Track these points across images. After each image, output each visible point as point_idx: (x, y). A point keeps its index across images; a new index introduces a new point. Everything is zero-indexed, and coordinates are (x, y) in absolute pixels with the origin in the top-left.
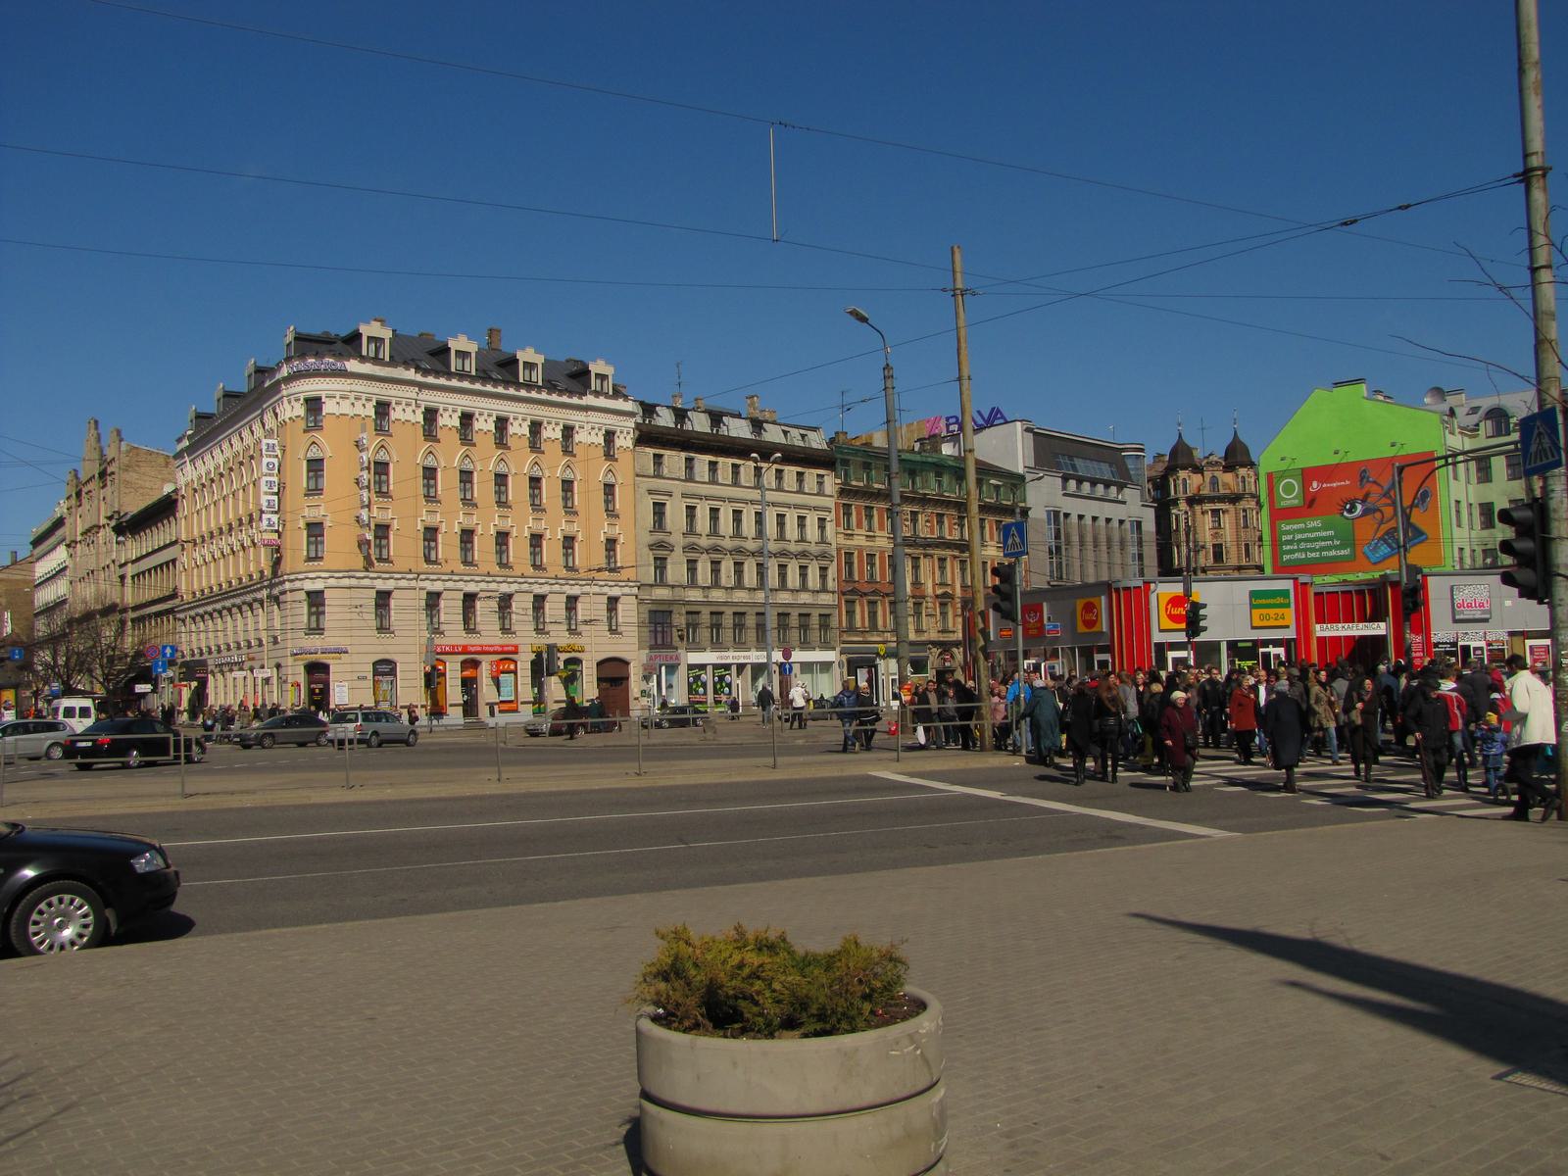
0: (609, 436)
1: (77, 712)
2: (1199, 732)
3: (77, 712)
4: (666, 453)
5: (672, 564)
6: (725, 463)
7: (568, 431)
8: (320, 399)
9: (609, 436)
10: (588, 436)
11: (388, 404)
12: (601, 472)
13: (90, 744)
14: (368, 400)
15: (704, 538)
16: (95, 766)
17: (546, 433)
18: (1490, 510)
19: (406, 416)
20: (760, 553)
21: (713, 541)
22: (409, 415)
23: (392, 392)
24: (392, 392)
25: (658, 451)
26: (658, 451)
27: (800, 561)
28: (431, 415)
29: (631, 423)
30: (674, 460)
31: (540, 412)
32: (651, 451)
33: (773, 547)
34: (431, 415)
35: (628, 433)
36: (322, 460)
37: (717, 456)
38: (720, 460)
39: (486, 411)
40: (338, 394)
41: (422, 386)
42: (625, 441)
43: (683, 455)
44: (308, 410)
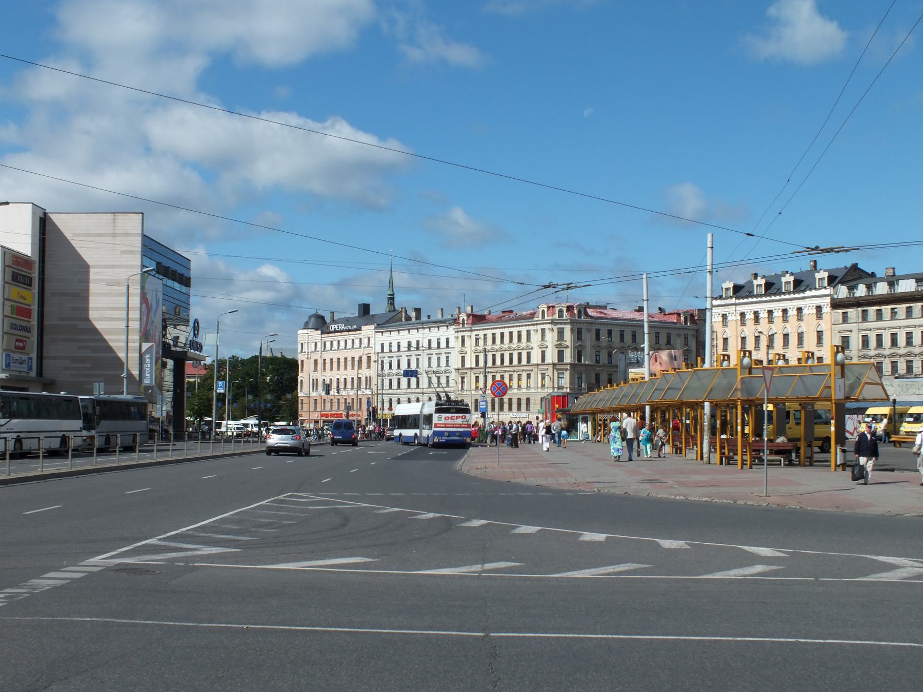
0: (819, 308)
1: (343, 425)
2: (680, 423)
3: (343, 425)
4: (849, 310)
5: (900, 362)
6: (902, 308)
7: (799, 310)
8: (821, 306)
9: (819, 308)
10: (809, 311)
11: (744, 313)
12: (825, 325)
13: (277, 423)
14: (779, 309)
15: (902, 348)
16: (410, 444)
17: (790, 313)
18: (65, 400)
19: (733, 318)
20: (909, 354)
21: (909, 349)
22: (734, 318)
23: (726, 310)
24: (726, 310)
25: (844, 311)
26: (844, 311)
27: (906, 358)
28: (743, 315)
29: (828, 300)
30: (853, 313)
31: (741, 309)
32: (840, 311)
33: (903, 351)
34: (743, 315)
35: (828, 305)
36: (745, 337)
37: (880, 306)
38: (883, 308)
39: (777, 308)
40: (777, 308)
41: (736, 304)
42: (827, 309)
43: (860, 309)
44: (817, 311)
